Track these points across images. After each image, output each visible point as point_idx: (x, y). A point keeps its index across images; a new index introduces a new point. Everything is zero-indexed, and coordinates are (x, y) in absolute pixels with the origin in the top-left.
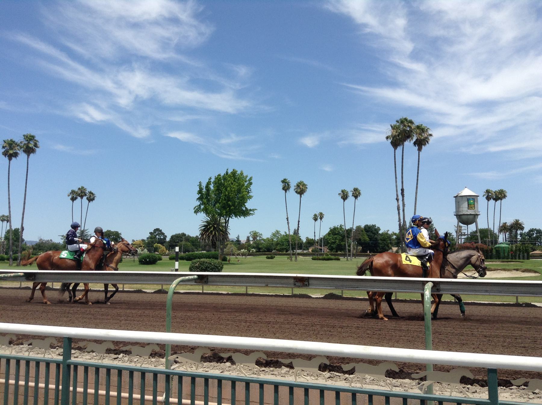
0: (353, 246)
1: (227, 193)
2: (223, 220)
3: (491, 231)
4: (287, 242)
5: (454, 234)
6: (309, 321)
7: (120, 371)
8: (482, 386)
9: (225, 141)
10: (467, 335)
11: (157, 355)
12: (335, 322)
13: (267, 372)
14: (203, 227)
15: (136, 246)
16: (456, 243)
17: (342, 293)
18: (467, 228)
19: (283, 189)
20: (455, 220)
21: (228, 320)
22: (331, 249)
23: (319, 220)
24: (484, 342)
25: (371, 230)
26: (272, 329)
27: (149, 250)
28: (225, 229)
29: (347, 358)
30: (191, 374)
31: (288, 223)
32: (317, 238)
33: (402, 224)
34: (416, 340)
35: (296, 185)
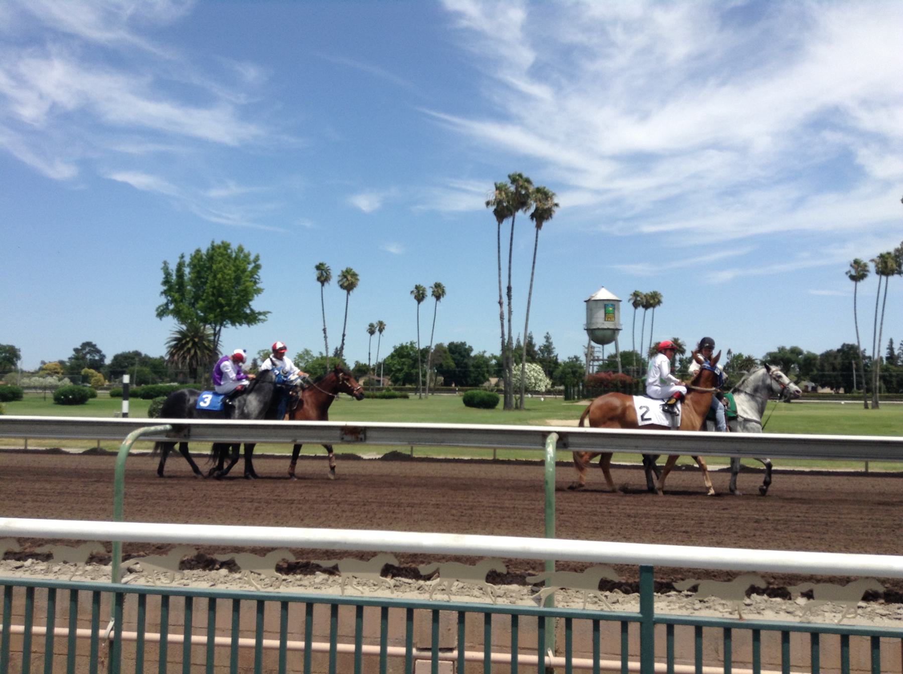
0: (431, 376)
1: (216, 283)
2: (209, 330)
3: (637, 355)
4: (323, 368)
5: (583, 359)
6: (358, 497)
7: (31, 589)
8: (626, 592)
9: (215, 193)
10: (603, 514)
11: (94, 559)
12: (401, 497)
13: (290, 582)
14: (175, 340)
15: (48, 372)
16: (585, 373)
17: (412, 451)
18: (603, 350)
19: (319, 279)
20: (585, 337)
21: (221, 499)
22: (395, 381)
23: (377, 333)
24: (627, 525)
25: (458, 351)
26: (298, 513)
27: (73, 380)
28: (214, 345)
29: (421, 554)
30: (724, 623)
31: (326, 337)
32: (373, 363)
33: (506, 341)
34: (527, 523)
35: (340, 273)
